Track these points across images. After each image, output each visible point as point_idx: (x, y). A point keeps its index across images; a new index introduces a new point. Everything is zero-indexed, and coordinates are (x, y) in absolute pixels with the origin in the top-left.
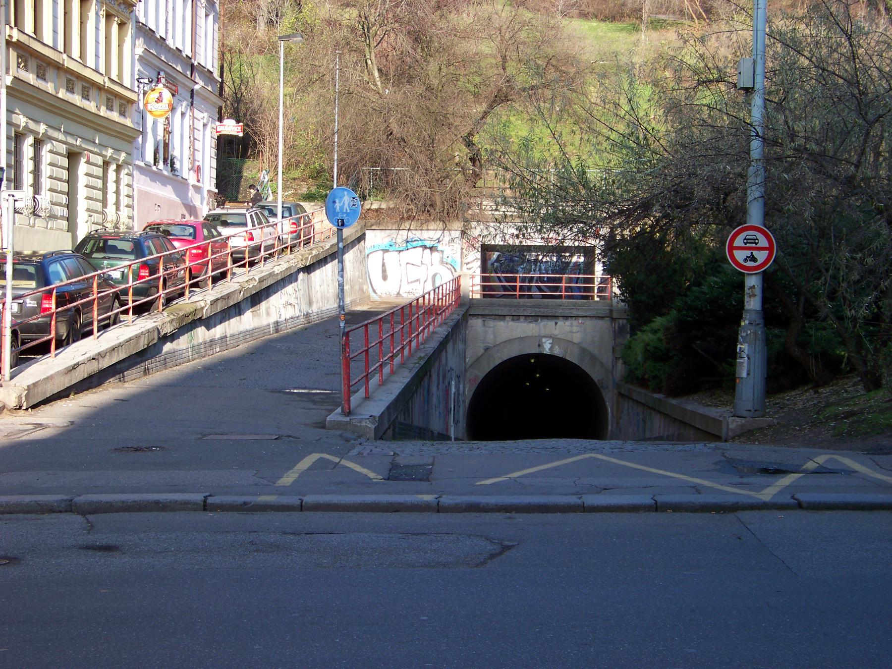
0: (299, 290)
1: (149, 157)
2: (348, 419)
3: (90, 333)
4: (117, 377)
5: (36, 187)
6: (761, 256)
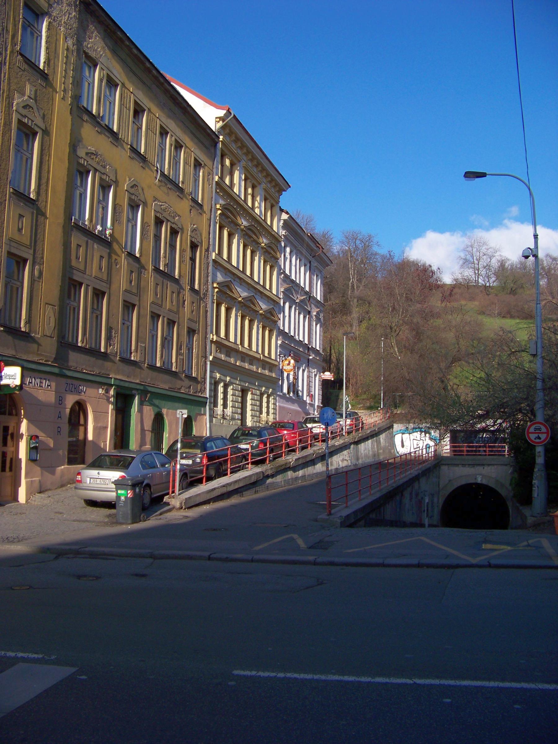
0: (351, 453)
1: (285, 390)
2: (328, 517)
3: (226, 474)
4: (239, 494)
5: (225, 406)
6: (543, 437)
